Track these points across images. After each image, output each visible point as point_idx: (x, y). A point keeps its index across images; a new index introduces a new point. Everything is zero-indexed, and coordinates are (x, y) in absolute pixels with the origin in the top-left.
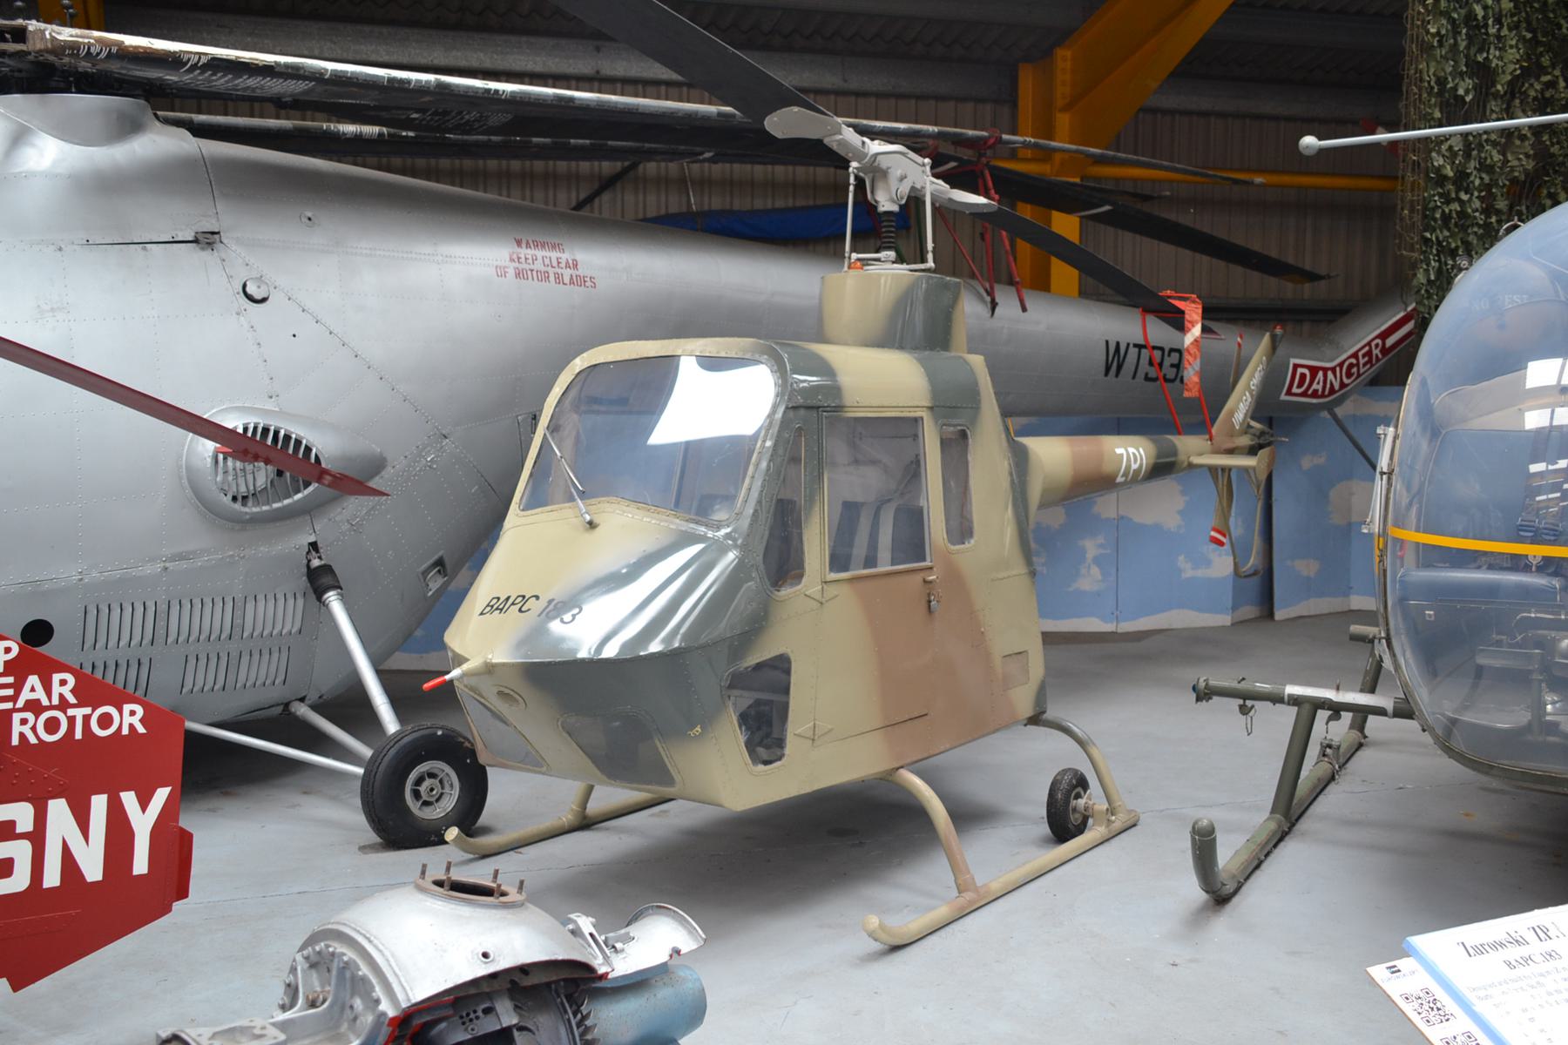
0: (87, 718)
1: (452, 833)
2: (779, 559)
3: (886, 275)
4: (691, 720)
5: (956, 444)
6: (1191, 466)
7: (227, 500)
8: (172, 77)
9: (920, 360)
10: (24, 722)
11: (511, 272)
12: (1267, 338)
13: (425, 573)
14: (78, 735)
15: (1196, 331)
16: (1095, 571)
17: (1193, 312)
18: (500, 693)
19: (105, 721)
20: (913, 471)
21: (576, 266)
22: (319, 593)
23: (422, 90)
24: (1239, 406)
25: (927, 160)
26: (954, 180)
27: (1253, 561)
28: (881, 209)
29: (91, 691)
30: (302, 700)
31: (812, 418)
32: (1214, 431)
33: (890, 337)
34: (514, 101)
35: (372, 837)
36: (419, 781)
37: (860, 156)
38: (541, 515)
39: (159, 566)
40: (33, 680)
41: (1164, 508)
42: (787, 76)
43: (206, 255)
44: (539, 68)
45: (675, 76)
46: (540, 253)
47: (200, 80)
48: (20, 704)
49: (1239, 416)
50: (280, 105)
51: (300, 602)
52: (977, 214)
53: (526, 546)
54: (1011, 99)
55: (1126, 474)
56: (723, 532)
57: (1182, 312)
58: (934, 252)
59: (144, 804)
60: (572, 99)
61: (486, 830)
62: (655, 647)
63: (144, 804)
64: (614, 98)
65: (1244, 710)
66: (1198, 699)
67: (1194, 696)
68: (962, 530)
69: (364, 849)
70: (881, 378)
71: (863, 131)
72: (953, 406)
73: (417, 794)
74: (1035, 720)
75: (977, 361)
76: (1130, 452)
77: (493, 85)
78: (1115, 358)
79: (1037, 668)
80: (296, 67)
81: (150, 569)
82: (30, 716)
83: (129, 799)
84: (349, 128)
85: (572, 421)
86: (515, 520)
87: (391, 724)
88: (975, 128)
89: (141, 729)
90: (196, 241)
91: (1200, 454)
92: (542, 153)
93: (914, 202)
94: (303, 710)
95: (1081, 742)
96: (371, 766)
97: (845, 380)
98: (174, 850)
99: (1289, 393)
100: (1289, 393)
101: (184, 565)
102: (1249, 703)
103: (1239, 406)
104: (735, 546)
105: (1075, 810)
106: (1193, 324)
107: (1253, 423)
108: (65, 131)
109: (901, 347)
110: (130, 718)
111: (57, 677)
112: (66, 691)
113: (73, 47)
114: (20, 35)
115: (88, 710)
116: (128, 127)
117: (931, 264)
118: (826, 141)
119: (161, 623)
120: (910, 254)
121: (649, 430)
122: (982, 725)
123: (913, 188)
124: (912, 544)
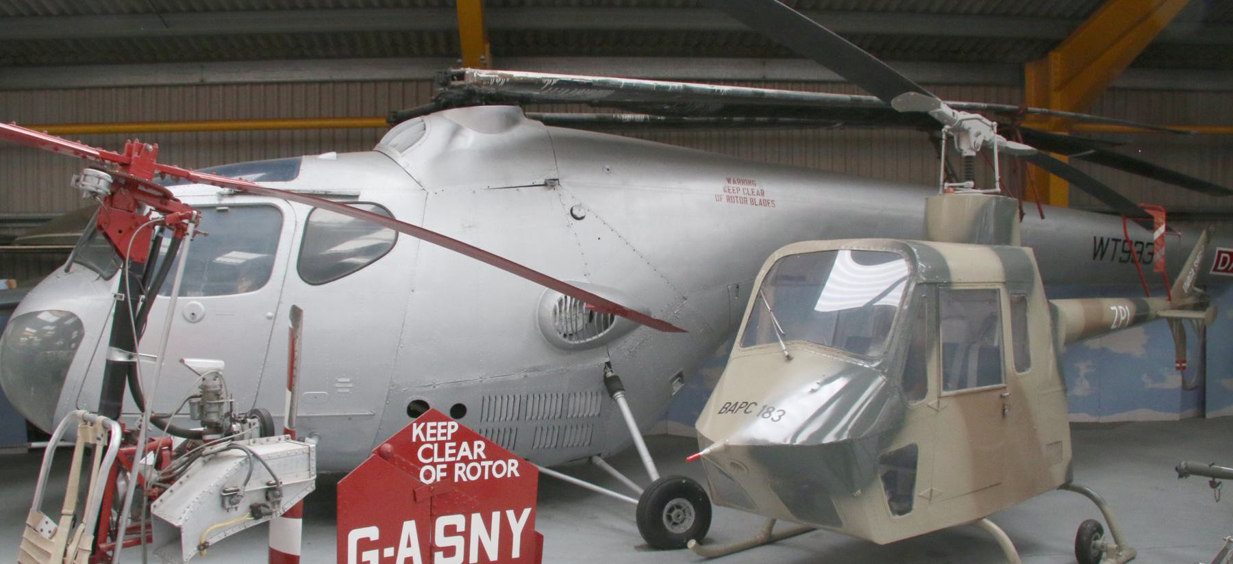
0: (490, 467)
1: (692, 543)
2: (911, 380)
3: (969, 198)
4: (850, 485)
5: (1020, 304)
6: (1158, 317)
7: (561, 336)
8: (536, 93)
9: (994, 250)
10: (460, 468)
11: (724, 198)
12: (1203, 235)
13: (673, 380)
14: (486, 477)
15: (1162, 229)
16: (1086, 383)
17: (1160, 218)
18: (732, 464)
19: (499, 469)
20: (992, 321)
21: (763, 194)
22: (611, 393)
23: (675, 92)
24: (1187, 278)
25: (995, 123)
26: (1009, 137)
27: (1193, 381)
28: (965, 155)
29: (494, 452)
30: (599, 455)
31: (934, 290)
32: (1172, 292)
33: (971, 238)
34: (729, 96)
35: (642, 541)
36: (671, 510)
37: (951, 122)
38: (753, 351)
39: (522, 375)
40: (465, 445)
41: (1134, 343)
42: (907, 73)
43: (551, 192)
44: (729, 76)
45: (841, 78)
46: (741, 187)
47: (550, 94)
48: (459, 458)
49: (1187, 284)
50: (592, 104)
51: (600, 397)
52: (1023, 157)
53: (743, 367)
54: (1021, 82)
55: (1118, 322)
56: (877, 364)
57: (1152, 217)
58: (1000, 181)
59: (518, 517)
60: (763, 94)
61: (711, 541)
62: (829, 438)
63: (518, 517)
64: (788, 92)
65: (1213, 485)
66: (1181, 476)
67: (1177, 474)
68: (1023, 362)
69: (639, 548)
70: (973, 264)
71: (953, 107)
72: (1016, 280)
73: (669, 518)
74: (1067, 486)
75: (1029, 251)
76: (1119, 309)
77: (716, 87)
78: (1100, 248)
79: (1067, 453)
80: (604, 83)
81: (516, 377)
82: (463, 465)
83: (510, 514)
84: (628, 117)
85: (770, 291)
86: (737, 351)
87: (654, 475)
88: (1010, 103)
89: (517, 474)
90: (545, 185)
91: (1165, 310)
92: (742, 125)
93: (986, 149)
94: (600, 461)
95: (1098, 502)
96: (643, 499)
97: (951, 264)
98: (533, 542)
99: (1215, 269)
100: (1215, 269)
101: (536, 374)
102: (1217, 480)
103: (1187, 278)
104: (883, 373)
105: (1094, 547)
106: (1160, 225)
107: (1197, 289)
108: (478, 127)
109: (979, 243)
110: (511, 467)
111: (476, 443)
112: (481, 451)
113: (488, 80)
114: (461, 76)
115: (491, 463)
116: (512, 122)
117: (998, 189)
118: (931, 112)
119: (523, 408)
120: (986, 184)
121: (815, 296)
122: (1031, 488)
123: (984, 141)
124: (991, 371)
